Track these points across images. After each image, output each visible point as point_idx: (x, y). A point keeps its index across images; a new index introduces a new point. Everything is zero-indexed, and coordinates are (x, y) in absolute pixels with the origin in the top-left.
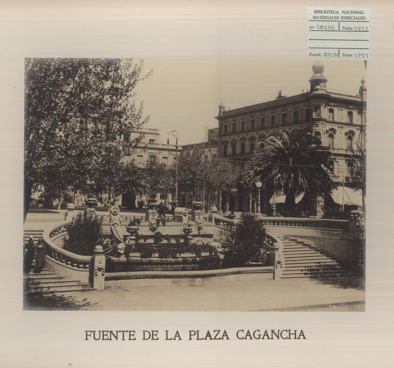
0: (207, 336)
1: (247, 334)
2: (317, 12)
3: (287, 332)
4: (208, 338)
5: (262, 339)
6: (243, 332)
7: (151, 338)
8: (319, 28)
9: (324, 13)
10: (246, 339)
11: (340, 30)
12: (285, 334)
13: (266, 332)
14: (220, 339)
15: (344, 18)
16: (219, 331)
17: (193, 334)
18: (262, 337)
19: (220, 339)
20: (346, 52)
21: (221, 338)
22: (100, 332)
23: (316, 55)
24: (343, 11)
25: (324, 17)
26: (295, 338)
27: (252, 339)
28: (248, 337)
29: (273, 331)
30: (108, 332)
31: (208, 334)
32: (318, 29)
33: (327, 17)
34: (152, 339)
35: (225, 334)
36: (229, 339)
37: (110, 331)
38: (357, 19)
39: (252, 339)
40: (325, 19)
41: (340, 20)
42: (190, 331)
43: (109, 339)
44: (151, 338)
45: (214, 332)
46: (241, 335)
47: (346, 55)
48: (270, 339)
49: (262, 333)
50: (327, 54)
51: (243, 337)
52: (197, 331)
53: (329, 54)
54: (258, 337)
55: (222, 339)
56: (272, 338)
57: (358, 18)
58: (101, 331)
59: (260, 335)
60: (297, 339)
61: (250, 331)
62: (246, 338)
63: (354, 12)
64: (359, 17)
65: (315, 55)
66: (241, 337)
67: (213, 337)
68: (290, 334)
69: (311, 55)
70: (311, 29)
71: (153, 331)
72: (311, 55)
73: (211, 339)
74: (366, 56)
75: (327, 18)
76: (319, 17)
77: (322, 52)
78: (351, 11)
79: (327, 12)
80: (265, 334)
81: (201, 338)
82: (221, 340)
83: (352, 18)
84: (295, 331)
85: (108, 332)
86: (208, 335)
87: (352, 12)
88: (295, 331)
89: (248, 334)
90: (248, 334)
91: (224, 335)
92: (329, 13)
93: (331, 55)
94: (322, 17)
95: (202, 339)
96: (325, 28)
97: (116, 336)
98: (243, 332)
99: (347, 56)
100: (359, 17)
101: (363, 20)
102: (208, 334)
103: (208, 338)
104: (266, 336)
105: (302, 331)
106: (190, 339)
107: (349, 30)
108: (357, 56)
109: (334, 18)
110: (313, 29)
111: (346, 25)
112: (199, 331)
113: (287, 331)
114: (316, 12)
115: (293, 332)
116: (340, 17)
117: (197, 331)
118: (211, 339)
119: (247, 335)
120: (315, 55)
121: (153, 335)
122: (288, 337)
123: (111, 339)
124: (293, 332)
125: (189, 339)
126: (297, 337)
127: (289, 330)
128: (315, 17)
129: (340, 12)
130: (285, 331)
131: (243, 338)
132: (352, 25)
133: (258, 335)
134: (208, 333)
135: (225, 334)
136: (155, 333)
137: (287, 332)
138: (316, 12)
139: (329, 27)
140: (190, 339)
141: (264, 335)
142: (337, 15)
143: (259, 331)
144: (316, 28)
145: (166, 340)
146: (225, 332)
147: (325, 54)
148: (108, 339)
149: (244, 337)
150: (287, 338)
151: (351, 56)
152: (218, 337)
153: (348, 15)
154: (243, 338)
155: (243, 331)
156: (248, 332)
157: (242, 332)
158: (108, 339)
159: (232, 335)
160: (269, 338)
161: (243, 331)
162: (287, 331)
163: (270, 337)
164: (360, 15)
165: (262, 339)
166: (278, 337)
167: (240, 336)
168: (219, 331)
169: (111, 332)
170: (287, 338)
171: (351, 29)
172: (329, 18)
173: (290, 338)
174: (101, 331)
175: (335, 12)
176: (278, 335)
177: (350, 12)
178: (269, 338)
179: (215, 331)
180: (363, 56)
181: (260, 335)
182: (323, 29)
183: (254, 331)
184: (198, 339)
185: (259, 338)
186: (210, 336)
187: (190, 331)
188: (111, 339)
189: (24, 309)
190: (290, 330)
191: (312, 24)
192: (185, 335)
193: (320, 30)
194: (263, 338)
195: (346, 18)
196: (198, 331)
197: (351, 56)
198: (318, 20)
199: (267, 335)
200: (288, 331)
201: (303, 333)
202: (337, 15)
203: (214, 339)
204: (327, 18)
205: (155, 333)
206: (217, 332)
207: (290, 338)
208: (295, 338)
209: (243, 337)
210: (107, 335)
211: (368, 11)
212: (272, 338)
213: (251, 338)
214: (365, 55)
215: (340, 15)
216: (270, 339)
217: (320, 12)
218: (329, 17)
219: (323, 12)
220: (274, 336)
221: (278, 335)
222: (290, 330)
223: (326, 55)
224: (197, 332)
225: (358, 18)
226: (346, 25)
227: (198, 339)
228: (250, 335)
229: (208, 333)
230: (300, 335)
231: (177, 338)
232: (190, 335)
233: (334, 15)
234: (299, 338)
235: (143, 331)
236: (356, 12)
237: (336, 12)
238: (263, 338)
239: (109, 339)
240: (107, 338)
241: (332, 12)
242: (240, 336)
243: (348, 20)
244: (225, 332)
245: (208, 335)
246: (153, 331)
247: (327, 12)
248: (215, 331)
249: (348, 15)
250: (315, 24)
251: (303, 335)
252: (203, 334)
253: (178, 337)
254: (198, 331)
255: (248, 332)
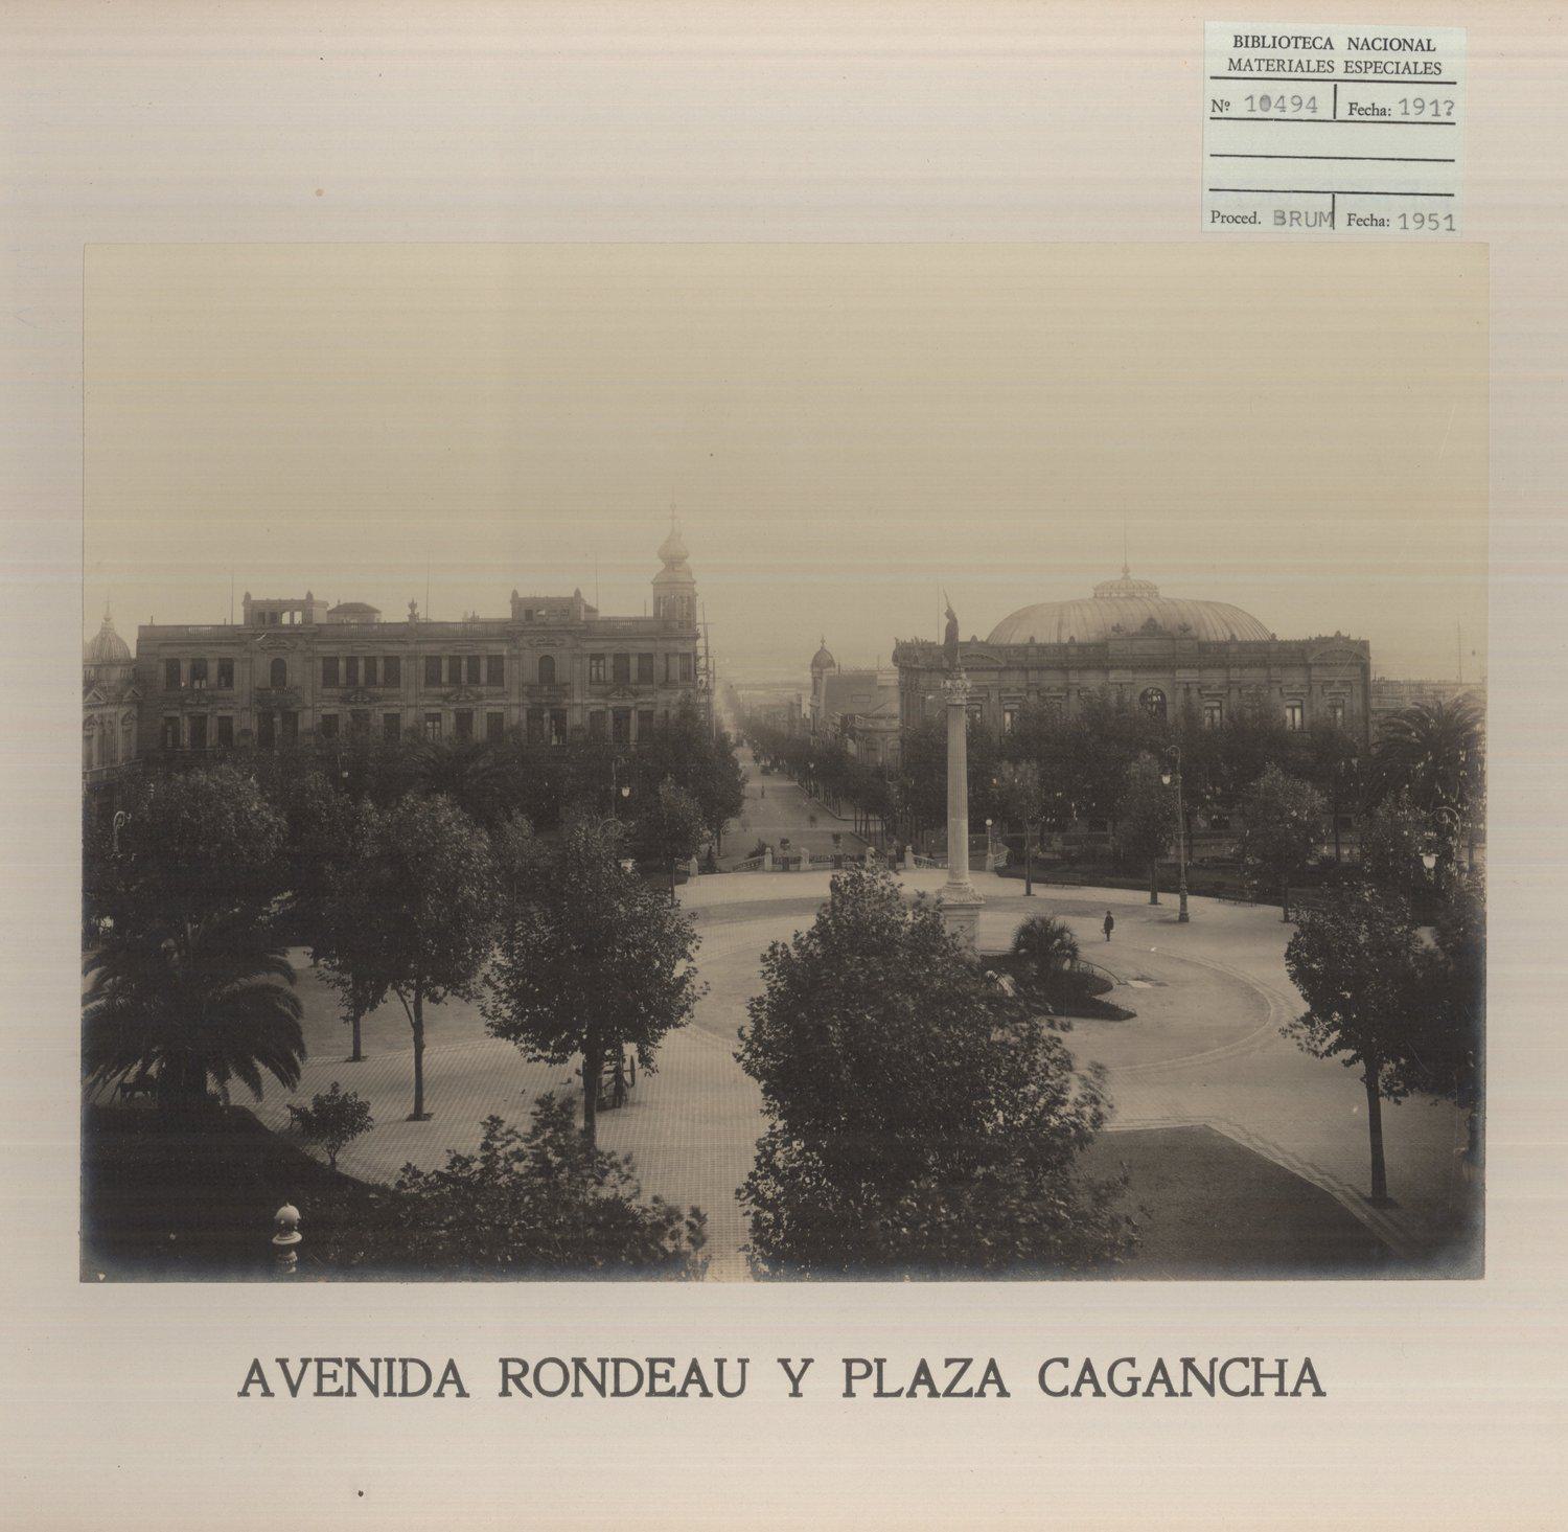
0: (917, 1381)
1: (689, 1374)
2: (1244, 41)
3: (1247, 1365)
4: (923, 1390)
5: (1145, 1395)
6: (1066, 1365)
7: (646, 1387)
8: (1256, 105)
9: (1274, 47)
10: (1299, 1394)
11: (1338, 118)
12: (1239, 1377)
13: (1160, 1366)
14: (969, 1393)
15: (1354, 67)
16: (968, 1362)
17: (860, 1370)
18: (1142, 1386)
19: (969, 1393)
20: (1364, 207)
21: (976, 1390)
22: (390, 1361)
23: (1239, 220)
24: (1350, 39)
25: (1276, 64)
26: (1281, 1392)
27: (1104, 1395)
28: (1087, 1389)
29: (1188, 1363)
30: (338, 1361)
31: (923, 1374)
32: (1437, 115)
33: (1287, 63)
34: (648, 1395)
35: (1160, 1376)
36: (1008, 1395)
37: (347, 1360)
38: (1248, 68)
39: (1104, 1395)
40: (1276, 71)
41: (1339, 73)
42: (849, 1362)
43: (346, 1390)
44: (646, 1387)
45: (946, 1366)
46: (1058, 1378)
47: (1361, 222)
48: (1176, 1395)
49: (1145, 1370)
50: (1288, 217)
51: (971, 1389)
52: (876, 1360)
53: (1296, 215)
54: (1126, 1386)
55: (981, 1394)
56: (1186, 1393)
57: (1305, 65)
58: (607, 1360)
59: (1134, 1380)
60: (1286, 1394)
61: (701, 1364)
62: (1077, 1393)
63: (1395, 44)
64: (1416, 63)
65: (1234, 219)
66: (1059, 1389)
67: (941, 1388)
68: (1258, 1376)
69: (1218, 220)
70: (1218, 114)
71: (652, 1362)
72: (1218, 220)
73: (933, 1393)
74: (1445, 224)
75: (1286, 67)
76: (1255, 65)
77: (1266, 206)
78: (1386, 40)
79: (1284, 42)
80: (446, 1374)
81: (894, 1391)
82: (973, 1400)
83: (1390, 68)
84: (1281, 1363)
85: (338, 1361)
86: (923, 1377)
87: (1388, 45)
88: (1281, 1363)
89: (694, 1377)
90: (694, 1377)
91: (986, 1381)
92: (1296, 47)
93: (1303, 222)
94: (1264, 65)
95: (898, 1394)
96: (1311, 105)
97: (599, 1380)
98: (1066, 1365)
99: (1368, 222)
100: (1416, 63)
101: (1430, 75)
102: (923, 1374)
103: (923, 1390)
104: (1160, 1381)
105: (1308, 1365)
106: (849, 1393)
107: (1377, 115)
108: (1411, 224)
109: (1314, 66)
110: (1225, 114)
111: (1365, 95)
112: (885, 1360)
113: (1245, 1361)
114: (1238, 41)
115: (1269, 1367)
116: (1340, 67)
117: (876, 1360)
118: (933, 1393)
119: (1081, 1380)
120: (1234, 219)
121: (653, 1375)
122: (1252, 1389)
123: (351, 1394)
124: (1269, 1367)
125: (844, 1395)
126: (1289, 1386)
127: (1253, 1359)
128: (1235, 61)
129: (1340, 43)
130: (1241, 1365)
131: (1065, 1392)
132: (1387, 97)
133: (1129, 1379)
134: (923, 1367)
135: (1087, 1376)
136: (660, 1368)
137: (1247, 1365)
138: (1238, 41)
139: (1297, 101)
140: (849, 1393)
141: (1154, 1380)
142: (1326, 55)
143: (1132, 1361)
144: (1239, 109)
145: (876, 1395)
146: (992, 1366)
147: (1279, 214)
148: (339, 1393)
149: (1072, 1389)
150: (1245, 1392)
151: (1382, 223)
152: (960, 1388)
153: (1372, 56)
154: (1065, 1392)
155: (1065, 1362)
156: (1088, 1366)
157: (1061, 1365)
158: (339, 1393)
159: (1020, 1378)
160: (1171, 1393)
161: (1065, 1362)
162: (1245, 1361)
163: (1178, 1387)
164: (1421, 57)
165: (1145, 1395)
166: (1210, 1389)
167: (1054, 1385)
168: (968, 1362)
169: (353, 1363)
170: (1245, 1392)
171: (1384, 112)
172: (1293, 68)
173: (1258, 1393)
174: (310, 1360)
175: (1319, 43)
176: (295, 1383)
177: (1378, 44)
178: (1171, 1393)
179: (948, 1362)
180: (1434, 225)
181: (1134, 1380)
182: (1274, 113)
183: (1231, 1357)
184: (880, 1393)
185: (1133, 1391)
186: (929, 1382)
187: (849, 1362)
188: (351, 1394)
189: (87, 1276)
190: (1258, 1361)
191: (1222, 90)
192: (482, 1378)
193: (1259, 114)
194: (1149, 1393)
195: (1363, 66)
196: (880, 1362)
197: (1382, 223)
198: (1251, 75)
199: (1166, 1380)
200: (1252, 1364)
201: (1165, 1373)
202: (1326, 55)
203: (948, 1393)
204: (1286, 67)
205: (660, 1368)
206: (957, 1367)
207: (1258, 1393)
208: (1281, 1392)
209: (971, 1389)
210: (334, 1376)
211: (1451, 44)
212: (1186, 1393)
213: (1098, 1393)
214: (1441, 220)
215: (1340, 55)
216: (1176, 1395)
217: (1258, 41)
218: (1401, 67)
219: (1269, 41)
220: (1194, 1384)
221: (295, 1383)
222: (1258, 1361)
223: (1280, 221)
224: (875, 1366)
225: (1305, 65)
226: (1365, 95)
227: (880, 1393)
228: (1094, 1381)
229: (923, 1367)
230: (1301, 1380)
231: (992, 1389)
232: (849, 1377)
233: (1314, 55)
234: (1296, 1393)
235: (844, 1360)
236: (1404, 44)
237: (1323, 43)
238: (1149, 1393)
239: (346, 1390)
240: (334, 1390)
241: (1307, 42)
242: (1054, 1385)
243: (1371, 75)
244: (992, 1366)
245: (923, 1377)
246: (652, 1362)
247: (1284, 42)
248: (948, 1362)
249: (1372, 56)
250: (1237, 94)
251: (457, 1381)
252: (899, 1375)
253: (1164, 1385)
254: (880, 1362)
255: (1088, 1366)
